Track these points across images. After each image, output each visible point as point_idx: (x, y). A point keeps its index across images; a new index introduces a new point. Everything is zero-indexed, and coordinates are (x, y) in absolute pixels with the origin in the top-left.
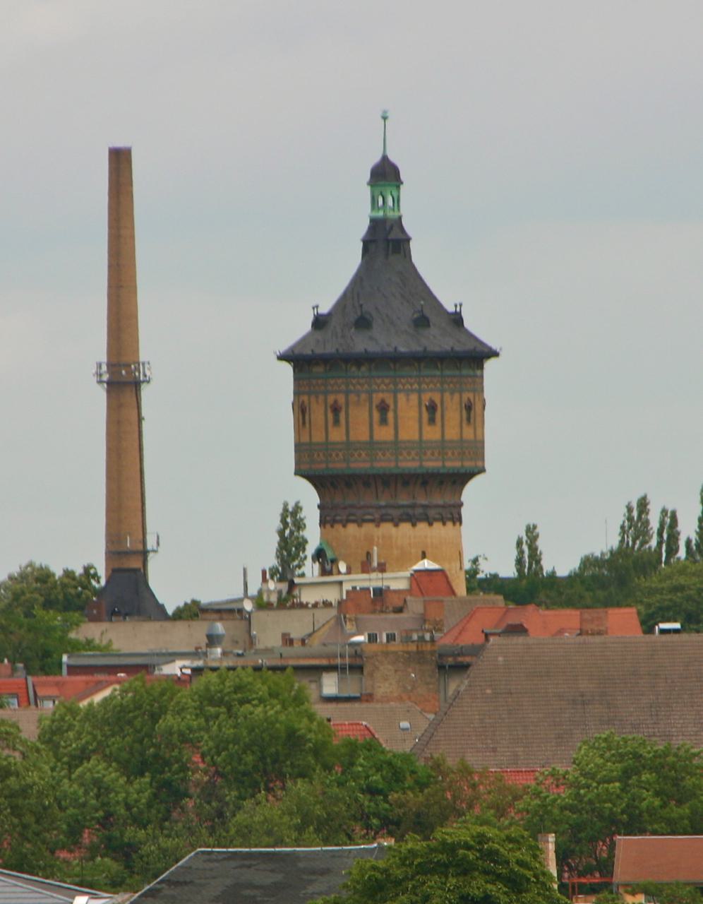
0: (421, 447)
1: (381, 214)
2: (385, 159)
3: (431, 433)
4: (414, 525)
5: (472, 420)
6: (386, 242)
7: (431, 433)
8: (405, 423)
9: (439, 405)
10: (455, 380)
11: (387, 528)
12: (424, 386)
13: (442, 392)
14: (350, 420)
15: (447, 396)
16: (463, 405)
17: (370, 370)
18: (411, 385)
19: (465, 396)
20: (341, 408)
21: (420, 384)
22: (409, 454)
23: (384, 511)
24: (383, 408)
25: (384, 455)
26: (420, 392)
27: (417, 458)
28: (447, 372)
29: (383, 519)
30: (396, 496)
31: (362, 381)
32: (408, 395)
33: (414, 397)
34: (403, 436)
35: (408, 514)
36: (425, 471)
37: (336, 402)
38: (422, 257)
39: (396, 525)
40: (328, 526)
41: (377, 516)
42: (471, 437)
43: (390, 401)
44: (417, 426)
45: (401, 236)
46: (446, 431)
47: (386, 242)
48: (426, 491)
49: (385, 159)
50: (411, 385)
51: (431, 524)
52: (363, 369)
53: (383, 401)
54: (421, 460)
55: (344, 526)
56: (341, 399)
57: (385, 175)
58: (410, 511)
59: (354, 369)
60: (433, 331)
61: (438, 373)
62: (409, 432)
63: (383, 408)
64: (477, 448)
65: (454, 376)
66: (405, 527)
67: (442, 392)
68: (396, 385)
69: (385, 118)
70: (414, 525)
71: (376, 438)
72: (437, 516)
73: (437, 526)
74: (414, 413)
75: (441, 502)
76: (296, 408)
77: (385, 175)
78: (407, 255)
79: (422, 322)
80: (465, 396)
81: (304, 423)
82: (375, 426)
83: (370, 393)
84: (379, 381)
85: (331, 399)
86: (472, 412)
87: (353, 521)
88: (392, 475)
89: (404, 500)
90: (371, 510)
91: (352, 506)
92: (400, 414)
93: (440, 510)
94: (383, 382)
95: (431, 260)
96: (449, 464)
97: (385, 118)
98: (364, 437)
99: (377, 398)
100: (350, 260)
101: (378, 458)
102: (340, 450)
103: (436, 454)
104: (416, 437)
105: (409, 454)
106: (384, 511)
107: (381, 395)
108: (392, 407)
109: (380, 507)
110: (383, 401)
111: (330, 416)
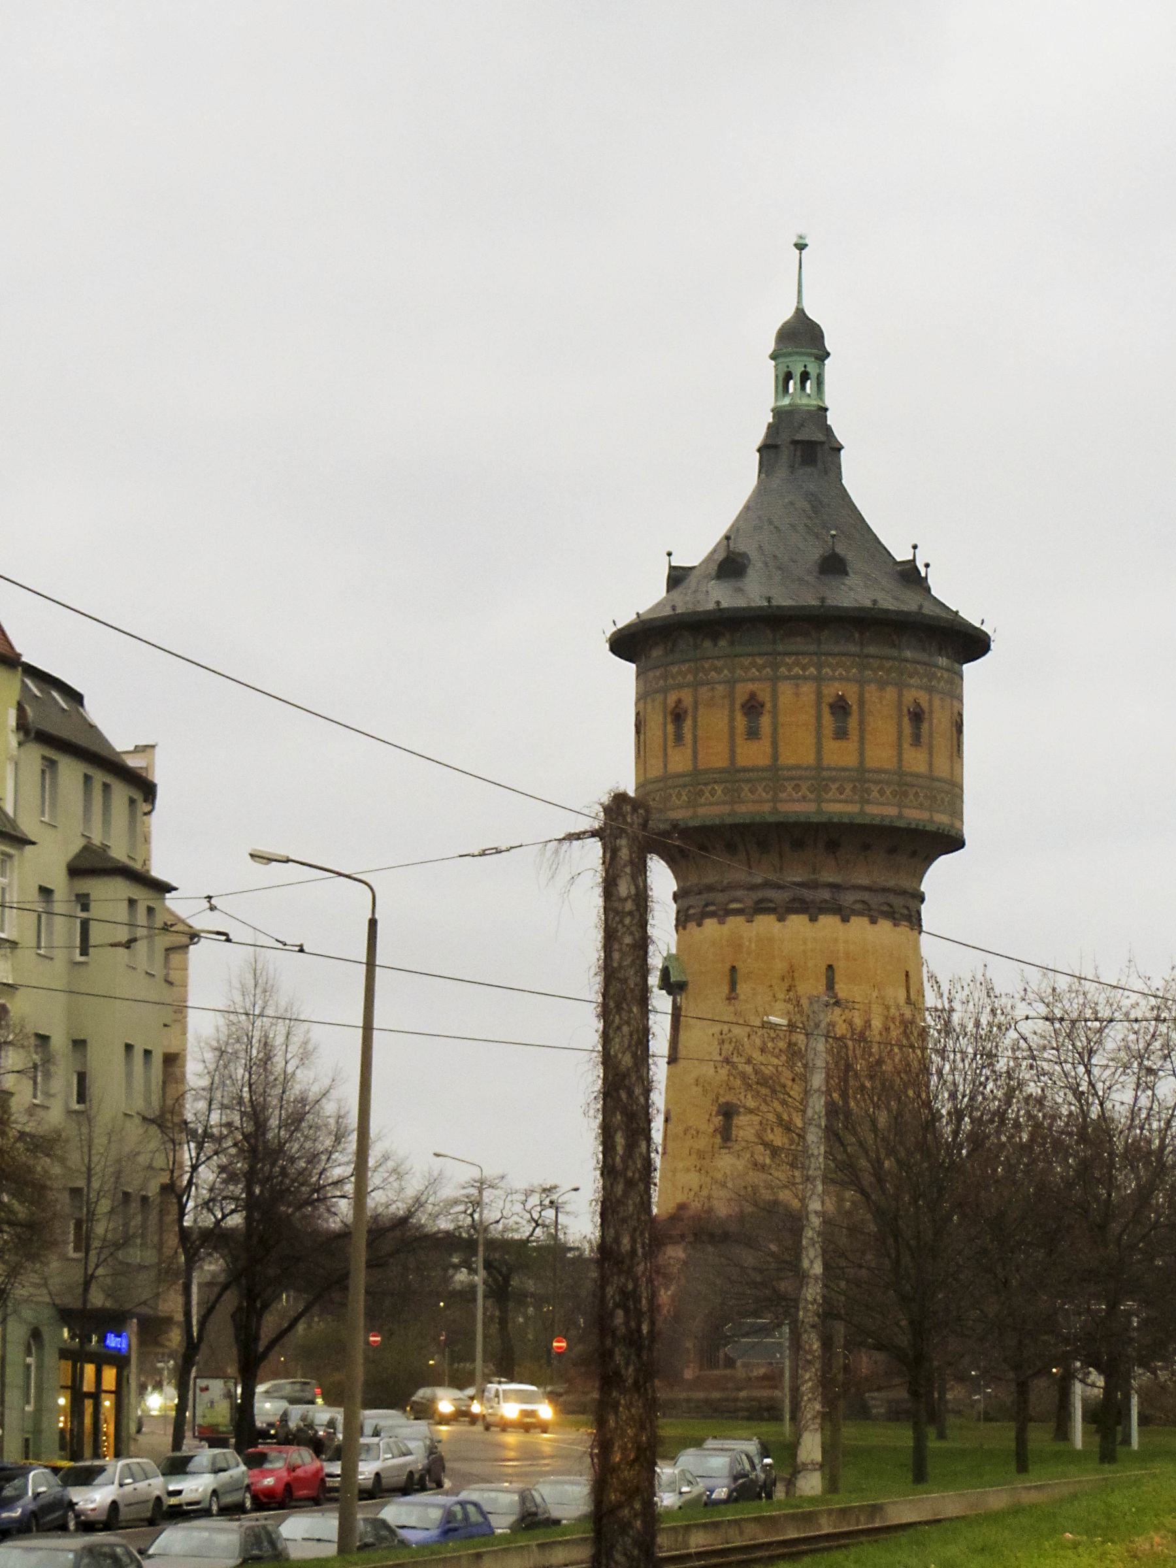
0: (820, 778)
1: (786, 401)
2: (800, 313)
3: (841, 754)
4: (813, 919)
5: (924, 739)
6: (800, 448)
7: (841, 754)
8: (799, 736)
9: (855, 707)
10: (888, 664)
11: (766, 924)
12: (827, 670)
13: (862, 683)
14: (700, 733)
15: (872, 691)
16: (905, 710)
17: (732, 643)
18: (804, 668)
19: (910, 696)
20: (686, 712)
21: (819, 667)
22: (797, 787)
23: (760, 894)
24: (753, 708)
25: (752, 791)
26: (819, 679)
27: (812, 796)
28: (872, 650)
29: (760, 908)
30: (781, 869)
31: (719, 663)
32: (797, 685)
33: (807, 689)
34: (788, 758)
35: (802, 901)
36: (824, 819)
37: (679, 701)
38: (859, 476)
39: (781, 919)
40: (692, 926)
41: (750, 903)
42: (922, 768)
43: (765, 696)
44: (811, 740)
45: (819, 437)
46: (868, 753)
47: (800, 448)
48: (836, 858)
49: (800, 313)
50: (804, 668)
51: (845, 920)
52: (722, 643)
53: (753, 696)
54: (819, 800)
55: (700, 925)
56: (687, 696)
57: (801, 341)
58: (808, 894)
59: (707, 644)
60: (853, 580)
61: (853, 649)
62: (798, 750)
63: (753, 708)
64: (950, 793)
65: (887, 658)
66: (797, 921)
67: (862, 683)
68: (775, 666)
69: (801, 247)
70: (813, 919)
71: (741, 762)
72: (858, 906)
73: (859, 924)
74: (808, 716)
75: (865, 881)
76: (655, 720)
77: (801, 341)
78: (833, 470)
79: (833, 566)
80: (910, 696)
81: (679, 738)
82: (739, 740)
83: (732, 683)
84: (746, 661)
85: (672, 699)
86: (925, 726)
87: (712, 915)
88: (769, 825)
89: (796, 875)
90: (740, 893)
91: (710, 888)
92: (782, 719)
93: (866, 896)
94: (754, 664)
95: (870, 480)
96: (872, 810)
97: (801, 247)
98: (721, 762)
99: (742, 691)
100: (741, 478)
101: (742, 795)
102: (888, 783)
103: (848, 791)
104: (810, 759)
105: (797, 787)
106: (760, 894)
107: (751, 686)
108: (768, 706)
109: (753, 888)
110: (753, 696)
111: (670, 728)
